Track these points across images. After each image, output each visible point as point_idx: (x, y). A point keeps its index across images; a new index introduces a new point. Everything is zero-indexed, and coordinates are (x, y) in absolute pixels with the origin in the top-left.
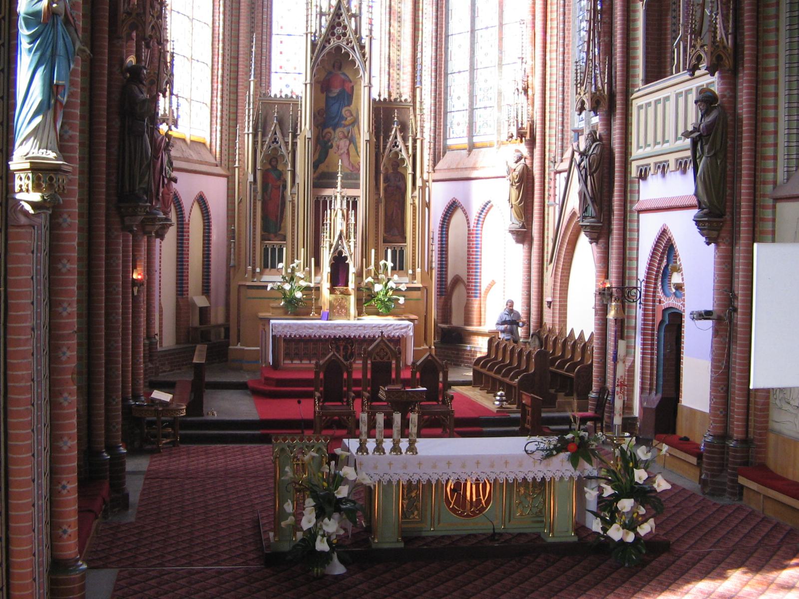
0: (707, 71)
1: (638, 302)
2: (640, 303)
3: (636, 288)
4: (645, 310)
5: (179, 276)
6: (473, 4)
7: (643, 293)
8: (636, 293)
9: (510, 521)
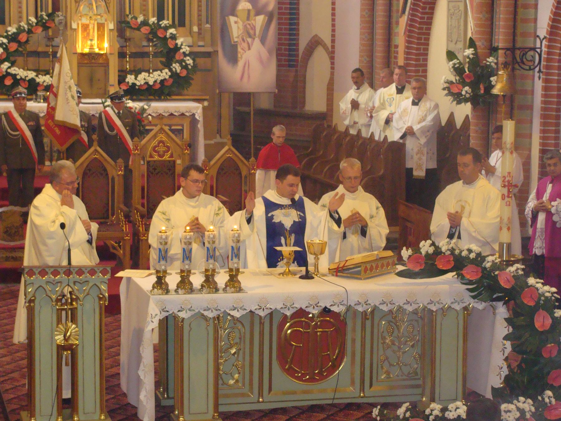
0: (107, 282)
1: (537, 69)
2: (540, 71)
3: (534, 49)
4: (546, 81)
5: (295, 35)
6: (333, 3)
7: (544, 56)
8: (533, 57)
9: (371, 386)
